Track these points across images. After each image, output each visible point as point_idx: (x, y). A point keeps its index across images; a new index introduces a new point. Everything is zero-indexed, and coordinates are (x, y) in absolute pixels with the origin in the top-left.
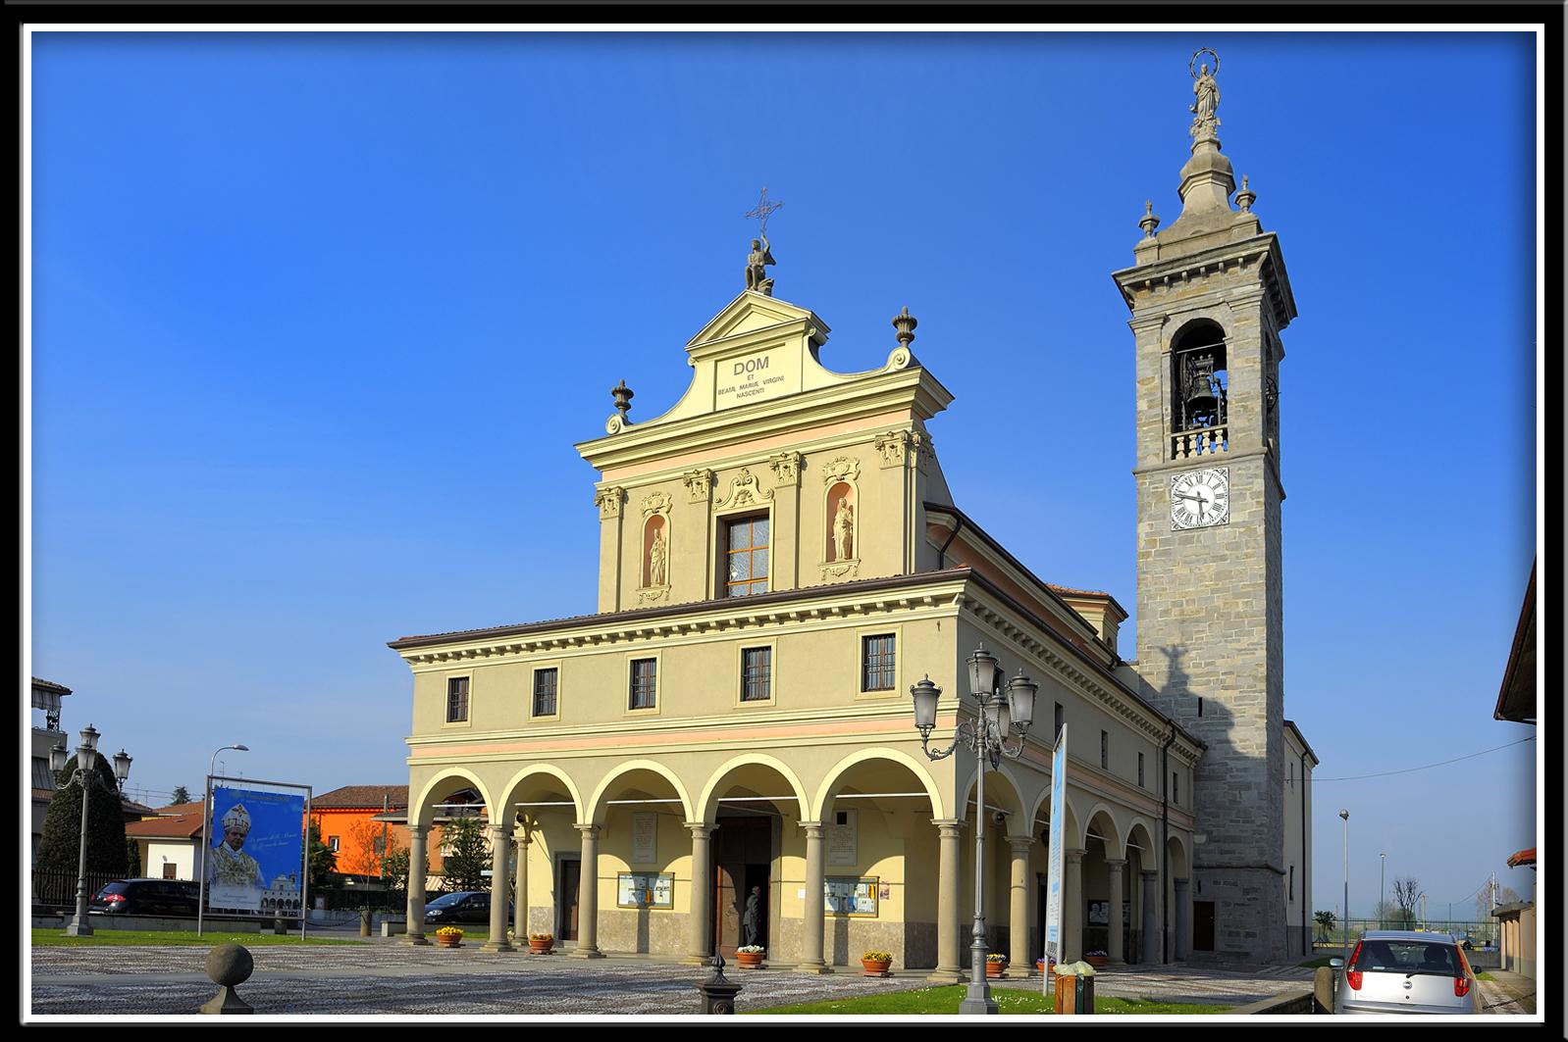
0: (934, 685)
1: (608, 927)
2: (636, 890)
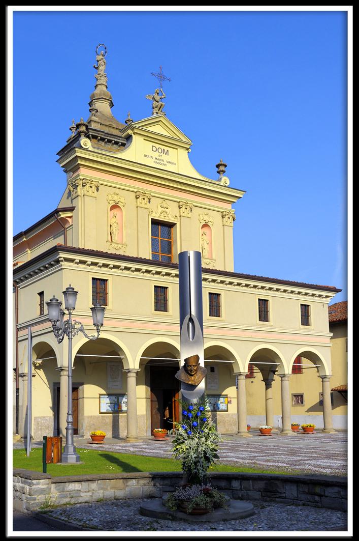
0: (58, 300)
1: (94, 425)
2: (111, 403)
